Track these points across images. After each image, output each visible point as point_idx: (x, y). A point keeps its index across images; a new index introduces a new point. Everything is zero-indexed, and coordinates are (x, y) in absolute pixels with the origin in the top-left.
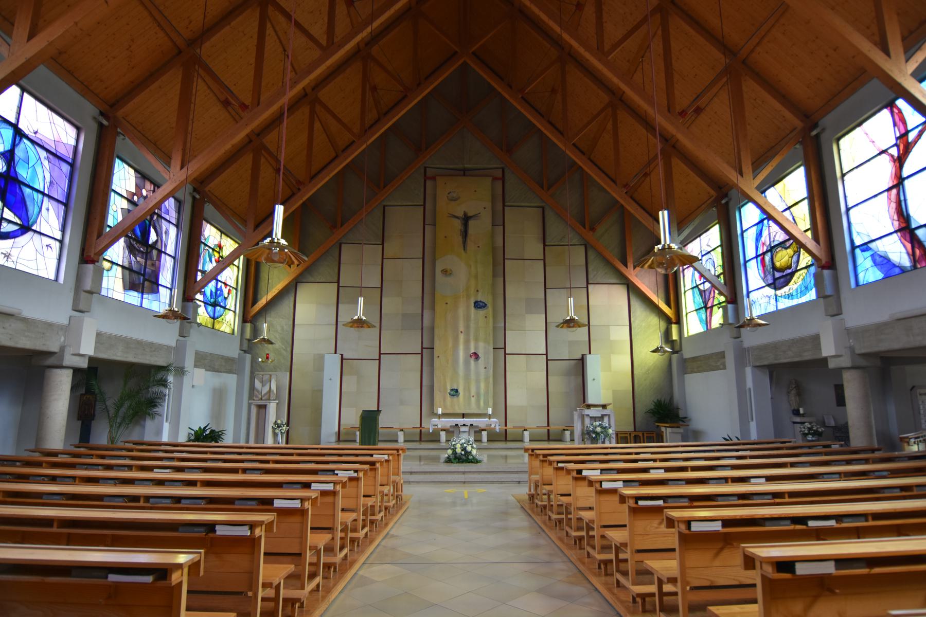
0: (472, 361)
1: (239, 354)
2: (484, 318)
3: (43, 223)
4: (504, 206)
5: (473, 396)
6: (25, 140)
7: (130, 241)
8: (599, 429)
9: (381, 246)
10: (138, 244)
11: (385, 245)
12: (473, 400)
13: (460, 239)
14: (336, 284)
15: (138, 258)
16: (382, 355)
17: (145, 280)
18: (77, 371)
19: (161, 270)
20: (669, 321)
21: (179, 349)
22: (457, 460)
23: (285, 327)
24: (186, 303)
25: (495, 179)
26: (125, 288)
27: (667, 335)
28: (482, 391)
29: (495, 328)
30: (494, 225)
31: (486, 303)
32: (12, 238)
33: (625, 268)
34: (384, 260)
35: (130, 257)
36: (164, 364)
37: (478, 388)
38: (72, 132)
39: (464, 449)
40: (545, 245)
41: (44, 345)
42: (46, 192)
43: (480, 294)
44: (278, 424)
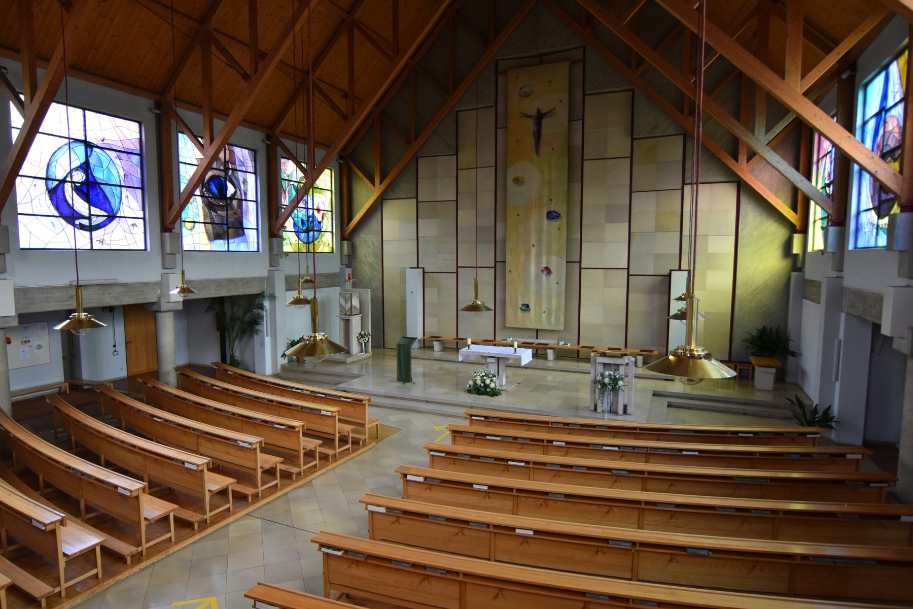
0: (544, 276)
1: (340, 269)
2: (558, 229)
3: (125, 208)
4: (584, 95)
5: (544, 312)
6: (95, 149)
7: (208, 200)
8: (607, 380)
9: (455, 156)
10: (217, 201)
11: (459, 154)
12: (544, 315)
13: (533, 141)
14: (415, 200)
15: (219, 212)
16: (493, 266)
17: (228, 228)
18: (177, 313)
19: (244, 216)
20: (793, 229)
21: (270, 279)
22: (476, 391)
23: (375, 242)
24: (272, 239)
25: (574, 62)
26: (210, 240)
27: (788, 246)
28: (554, 307)
29: (569, 240)
30: (570, 120)
31: (560, 213)
32: (103, 227)
33: (735, 162)
34: (459, 171)
35: (211, 213)
36: (259, 292)
37: (549, 304)
38: (134, 126)
39: (483, 382)
40: (633, 139)
41: (144, 299)
42: (123, 184)
43: (553, 203)
44: (362, 335)
